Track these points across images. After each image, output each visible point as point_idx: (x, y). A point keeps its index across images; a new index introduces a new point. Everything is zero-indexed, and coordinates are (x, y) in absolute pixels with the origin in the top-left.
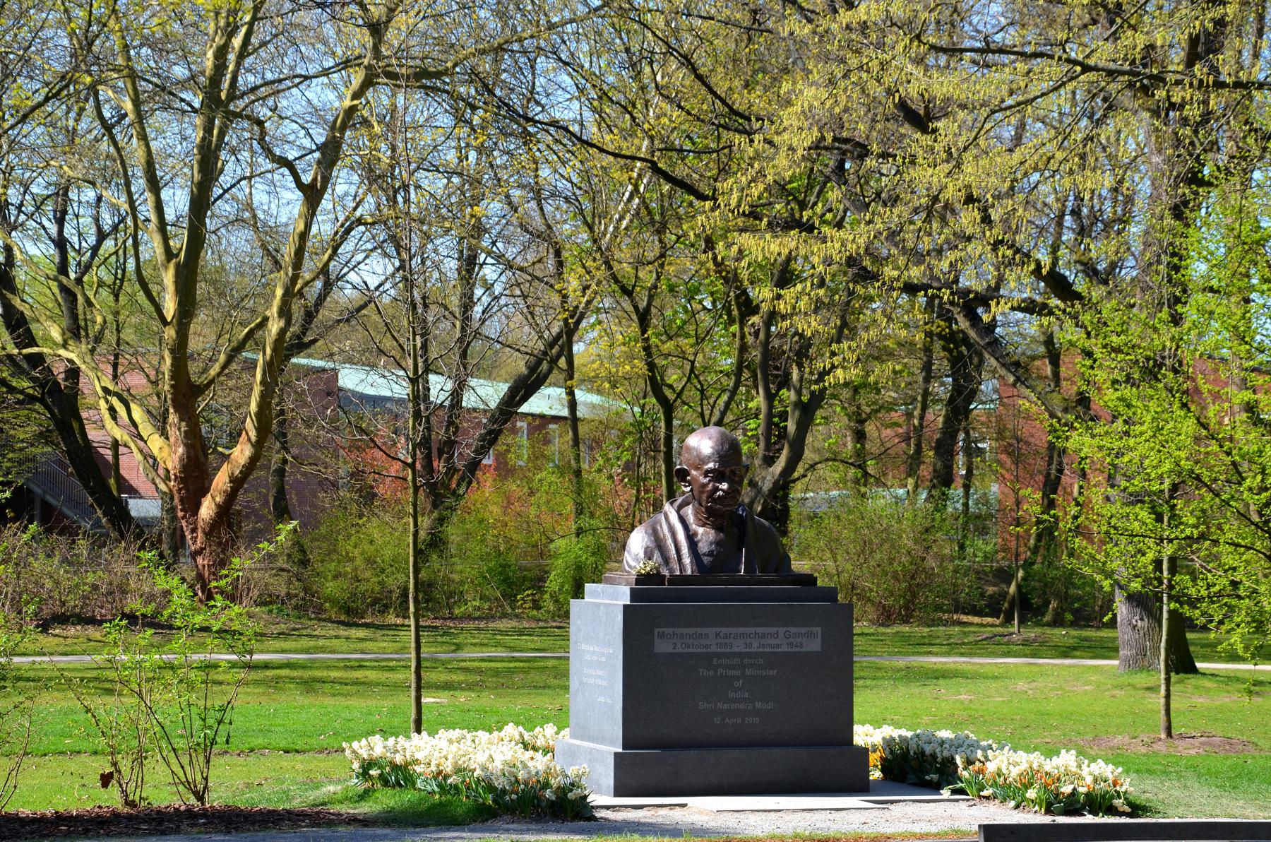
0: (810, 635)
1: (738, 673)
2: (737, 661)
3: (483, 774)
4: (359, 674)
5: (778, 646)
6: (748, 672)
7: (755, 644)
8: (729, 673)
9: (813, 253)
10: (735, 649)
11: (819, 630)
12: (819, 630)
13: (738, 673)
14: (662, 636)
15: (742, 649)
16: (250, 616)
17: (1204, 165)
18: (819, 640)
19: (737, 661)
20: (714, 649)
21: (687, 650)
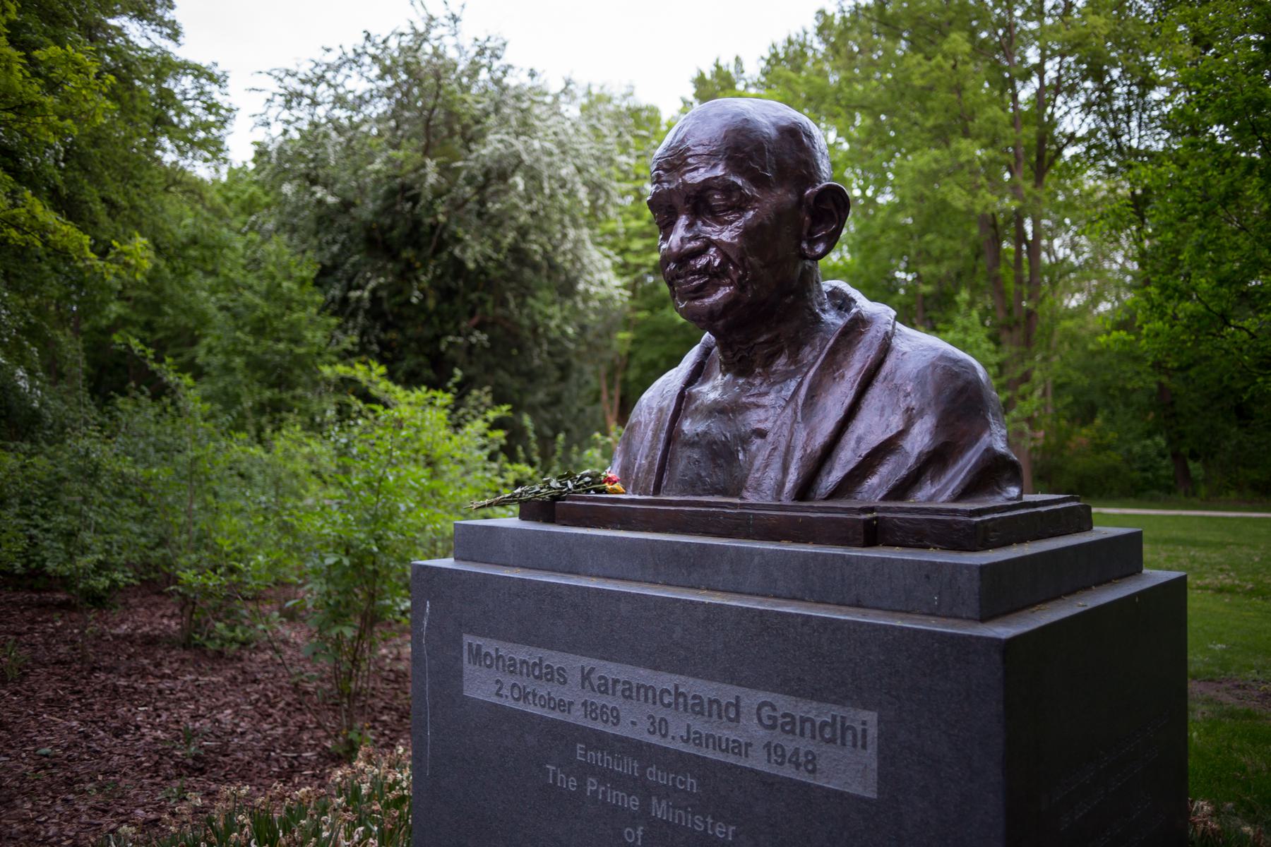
0: (839, 734)
1: (633, 803)
2: (630, 767)
3: (528, 82)
4: (859, 736)
5: (739, 748)
6: (659, 810)
7: (679, 724)
8: (615, 797)
9: (299, 568)
10: (622, 730)
11: (871, 717)
12: (871, 717)
13: (633, 803)
14: (477, 655)
15: (641, 734)
16: (302, 673)
17: (266, 661)
18: (870, 757)
19: (630, 767)
20: (577, 717)
21: (520, 706)
